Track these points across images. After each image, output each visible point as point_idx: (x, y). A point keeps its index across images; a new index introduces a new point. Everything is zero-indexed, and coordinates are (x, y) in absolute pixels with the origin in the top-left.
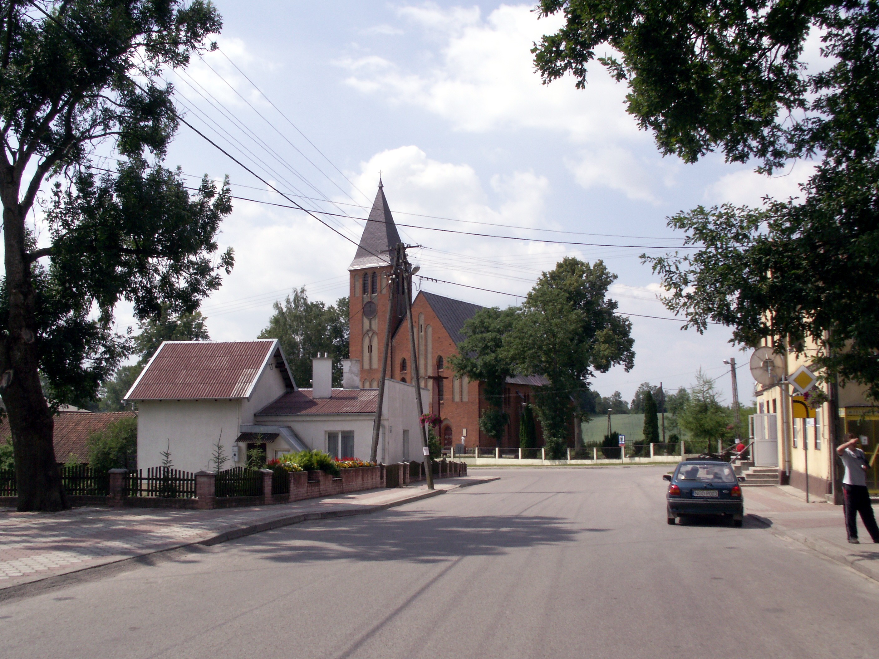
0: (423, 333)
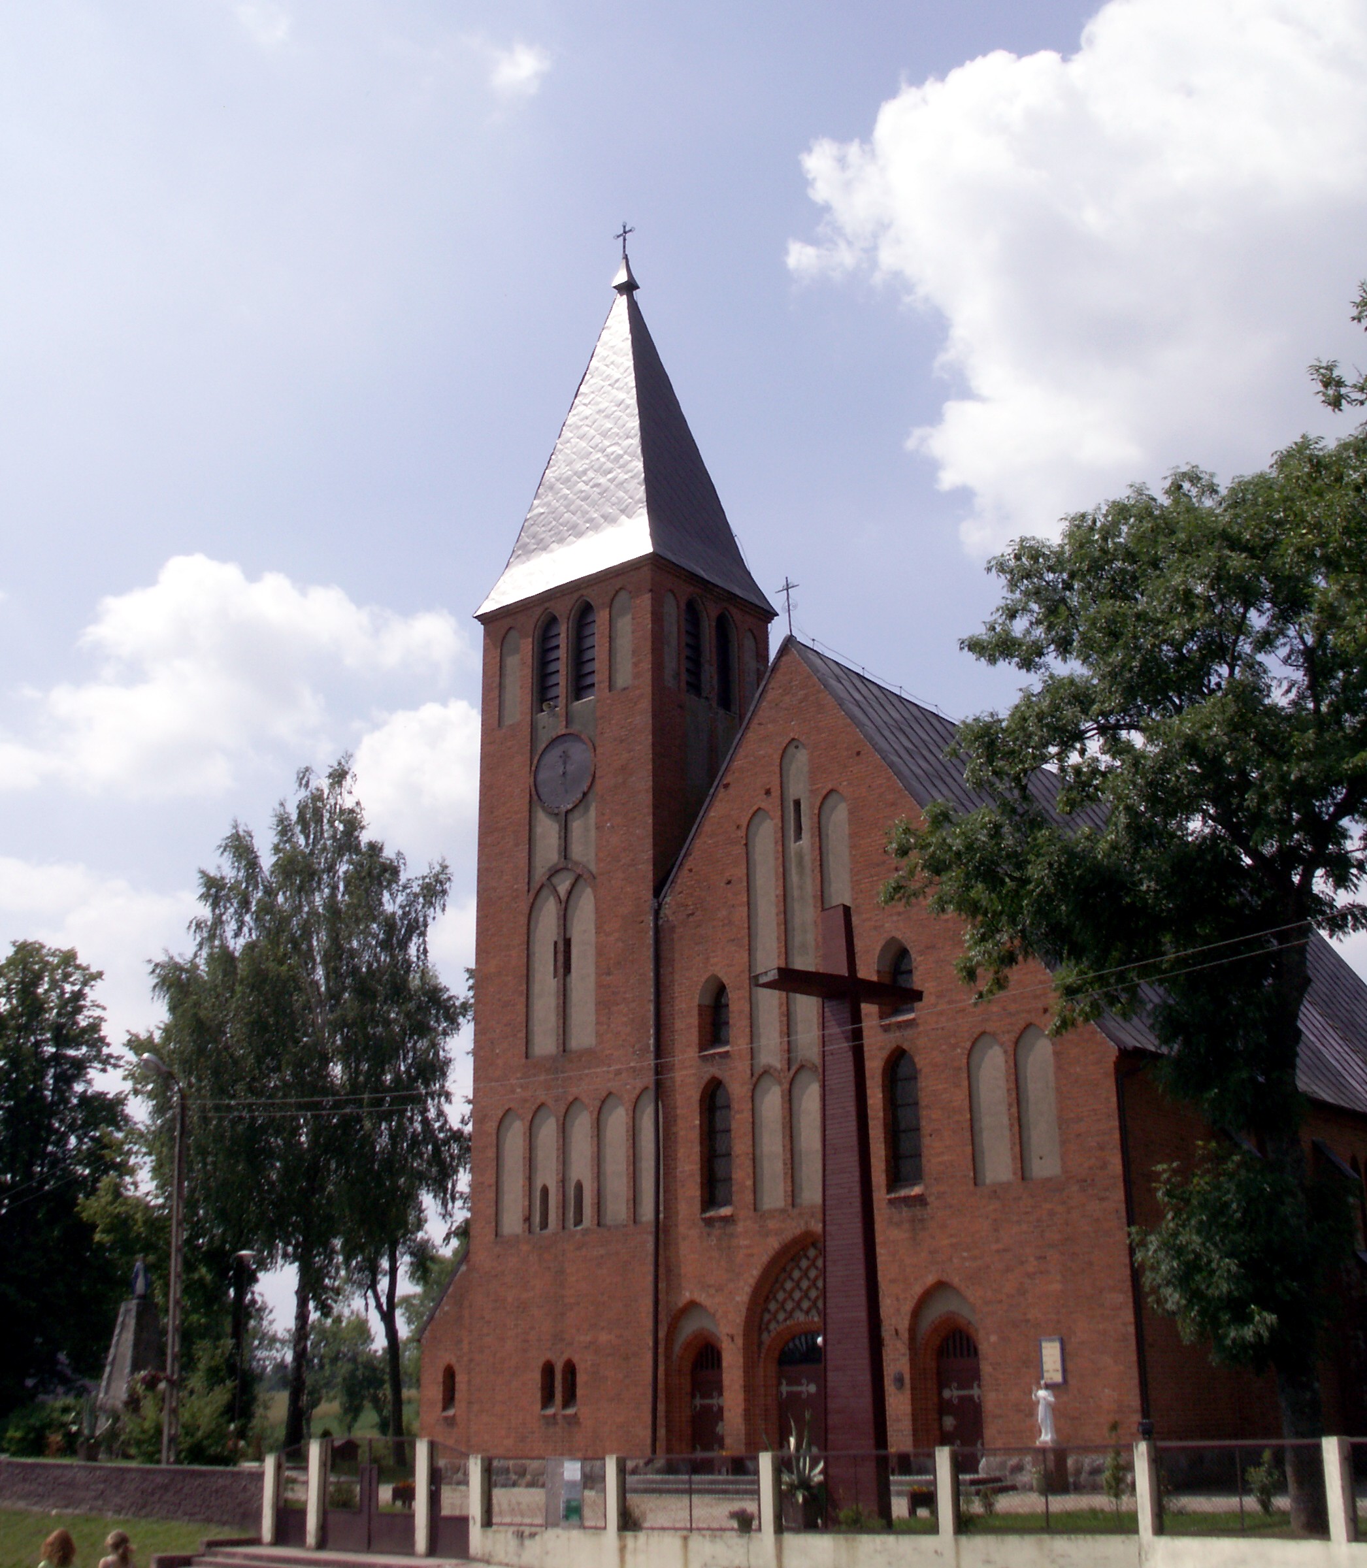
0: (806, 841)
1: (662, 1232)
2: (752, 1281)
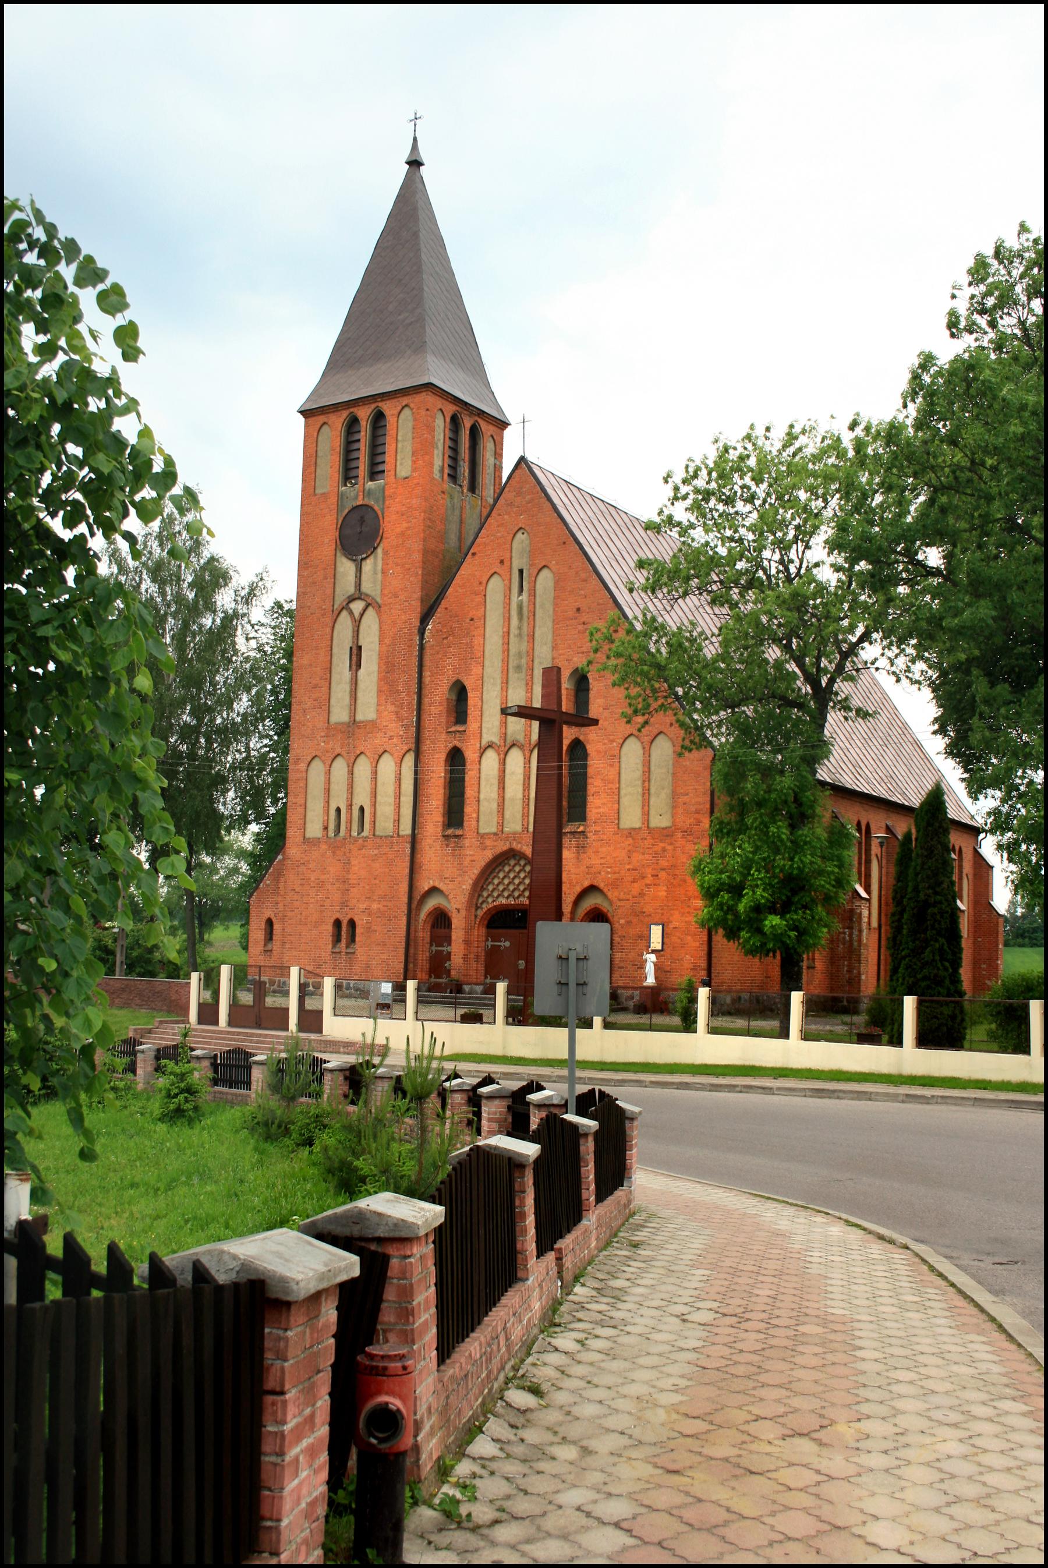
0: (525, 596)
1: (414, 840)
2: (474, 877)
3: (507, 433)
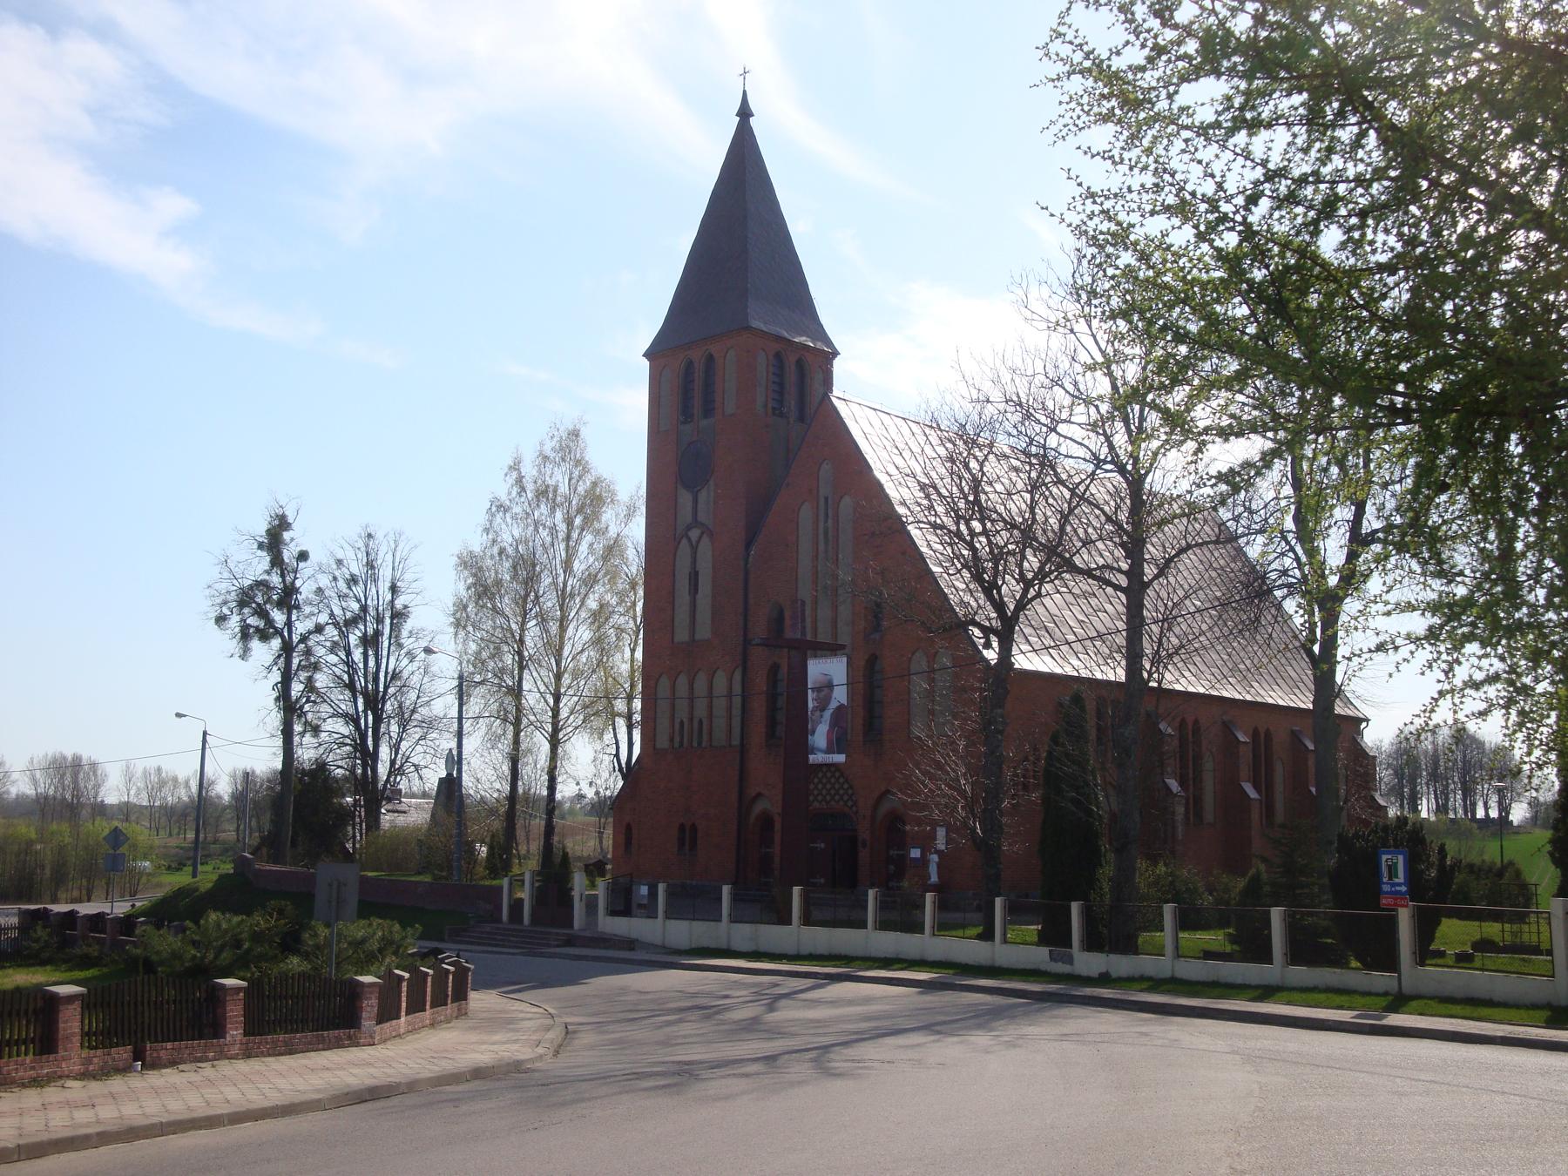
1: (743, 749)
3: (837, 363)
